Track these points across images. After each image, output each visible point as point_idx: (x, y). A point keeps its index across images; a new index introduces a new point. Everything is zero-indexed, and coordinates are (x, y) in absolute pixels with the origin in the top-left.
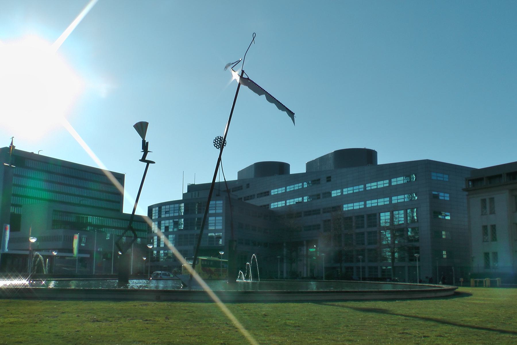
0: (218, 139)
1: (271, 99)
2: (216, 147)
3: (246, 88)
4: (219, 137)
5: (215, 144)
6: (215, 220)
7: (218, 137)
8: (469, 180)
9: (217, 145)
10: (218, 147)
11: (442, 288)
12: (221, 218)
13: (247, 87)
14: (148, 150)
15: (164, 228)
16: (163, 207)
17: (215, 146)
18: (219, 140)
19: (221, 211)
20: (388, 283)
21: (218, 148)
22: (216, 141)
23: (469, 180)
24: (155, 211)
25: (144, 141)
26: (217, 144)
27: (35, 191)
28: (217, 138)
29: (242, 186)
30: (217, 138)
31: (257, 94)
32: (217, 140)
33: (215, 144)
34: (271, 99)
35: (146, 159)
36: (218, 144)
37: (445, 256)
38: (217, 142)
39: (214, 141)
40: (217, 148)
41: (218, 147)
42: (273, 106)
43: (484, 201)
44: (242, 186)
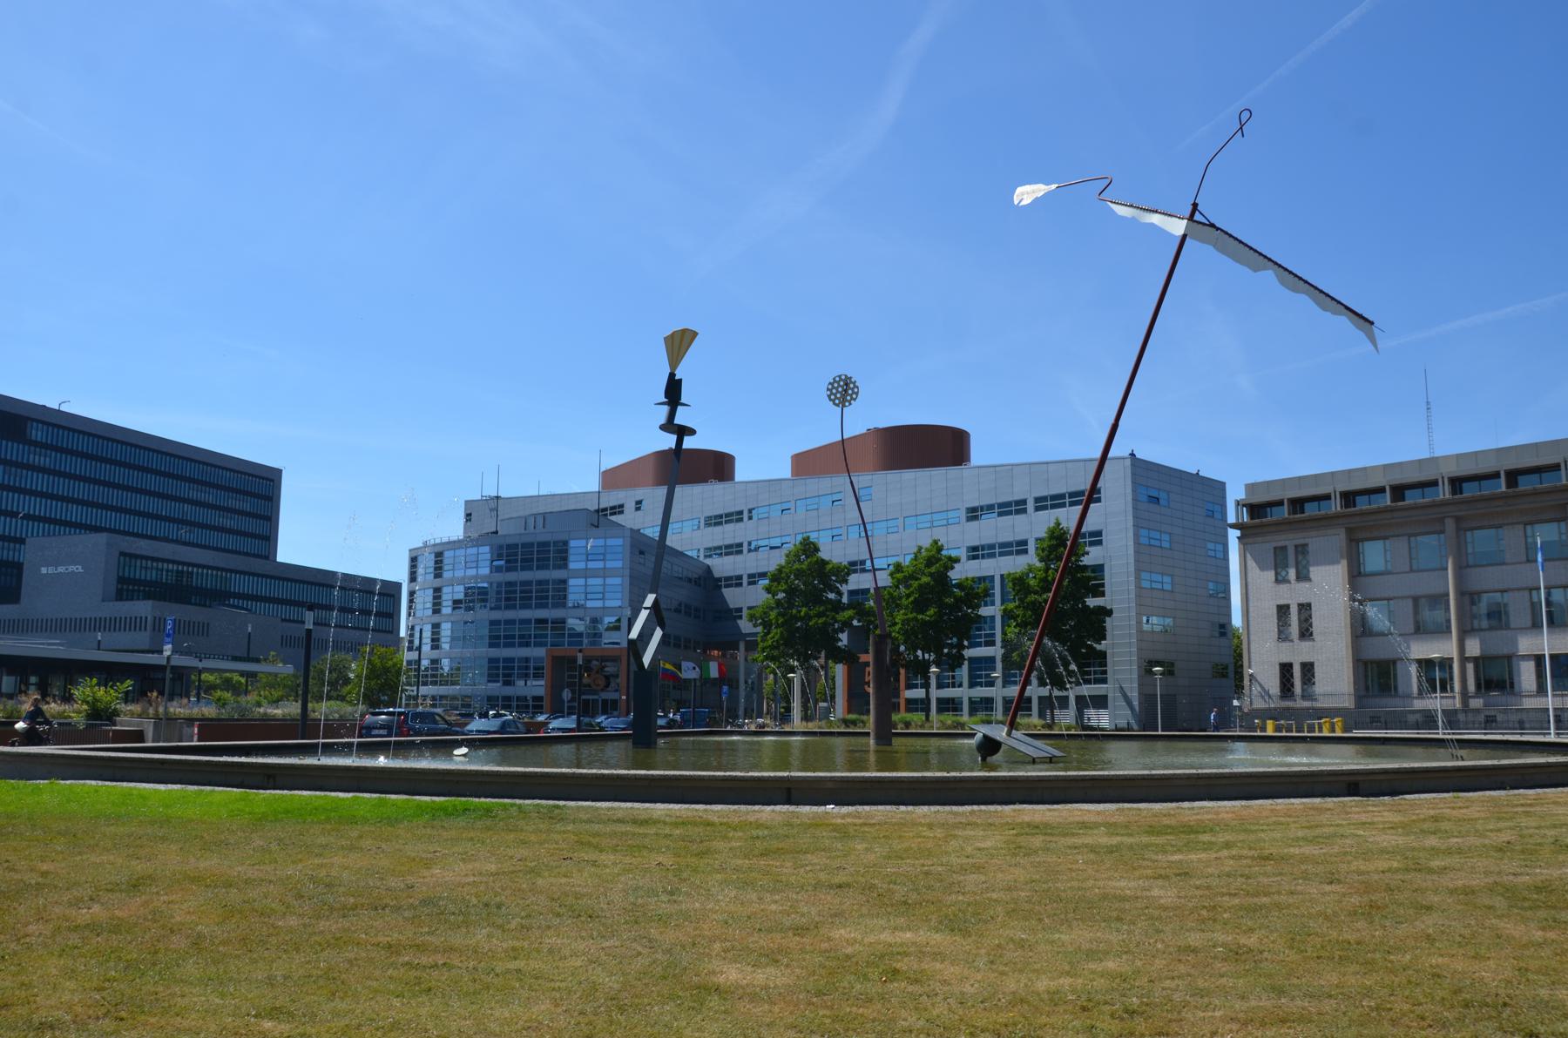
0: (838, 382)
1: (1294, 280)
2: (833, 401)
3: (1208, 250)
4: (843, 377)
5: (832, 393)
6: (586, 585)
7: (840, 376)
8: (1244, 505)
9: (836, 398)
10: (837, 401)
11: (1048, 742)
12: (618, 581)
13: (1211, 247)
14: (683, 401)
15: (450, 603)
16: (448, 554)
17: (830, 400)
18: (842, 383)
19: (619, 564)
20: (1242, 759)
21: (837, 405)
22: (833, 387)
23: (1244, 505)
24: (426, 565)
25: (672, 375)
26: (835, 395)
27: (143, 497)
28: (837, 379)
29: (622, 506)
30: (837, 379)
31: (1246, 269)
32: (836, 385)
33: (832, 393)
34: (1294, 280)
35: (677, 421)
36: (838, 395)
37: (250, 625)
38: (837, 388)
39: (830, 387)
40: (835, 404)
41: (837, 401)
42: (1304, 301)
43: (1280, 552)
44: (622, 506)
